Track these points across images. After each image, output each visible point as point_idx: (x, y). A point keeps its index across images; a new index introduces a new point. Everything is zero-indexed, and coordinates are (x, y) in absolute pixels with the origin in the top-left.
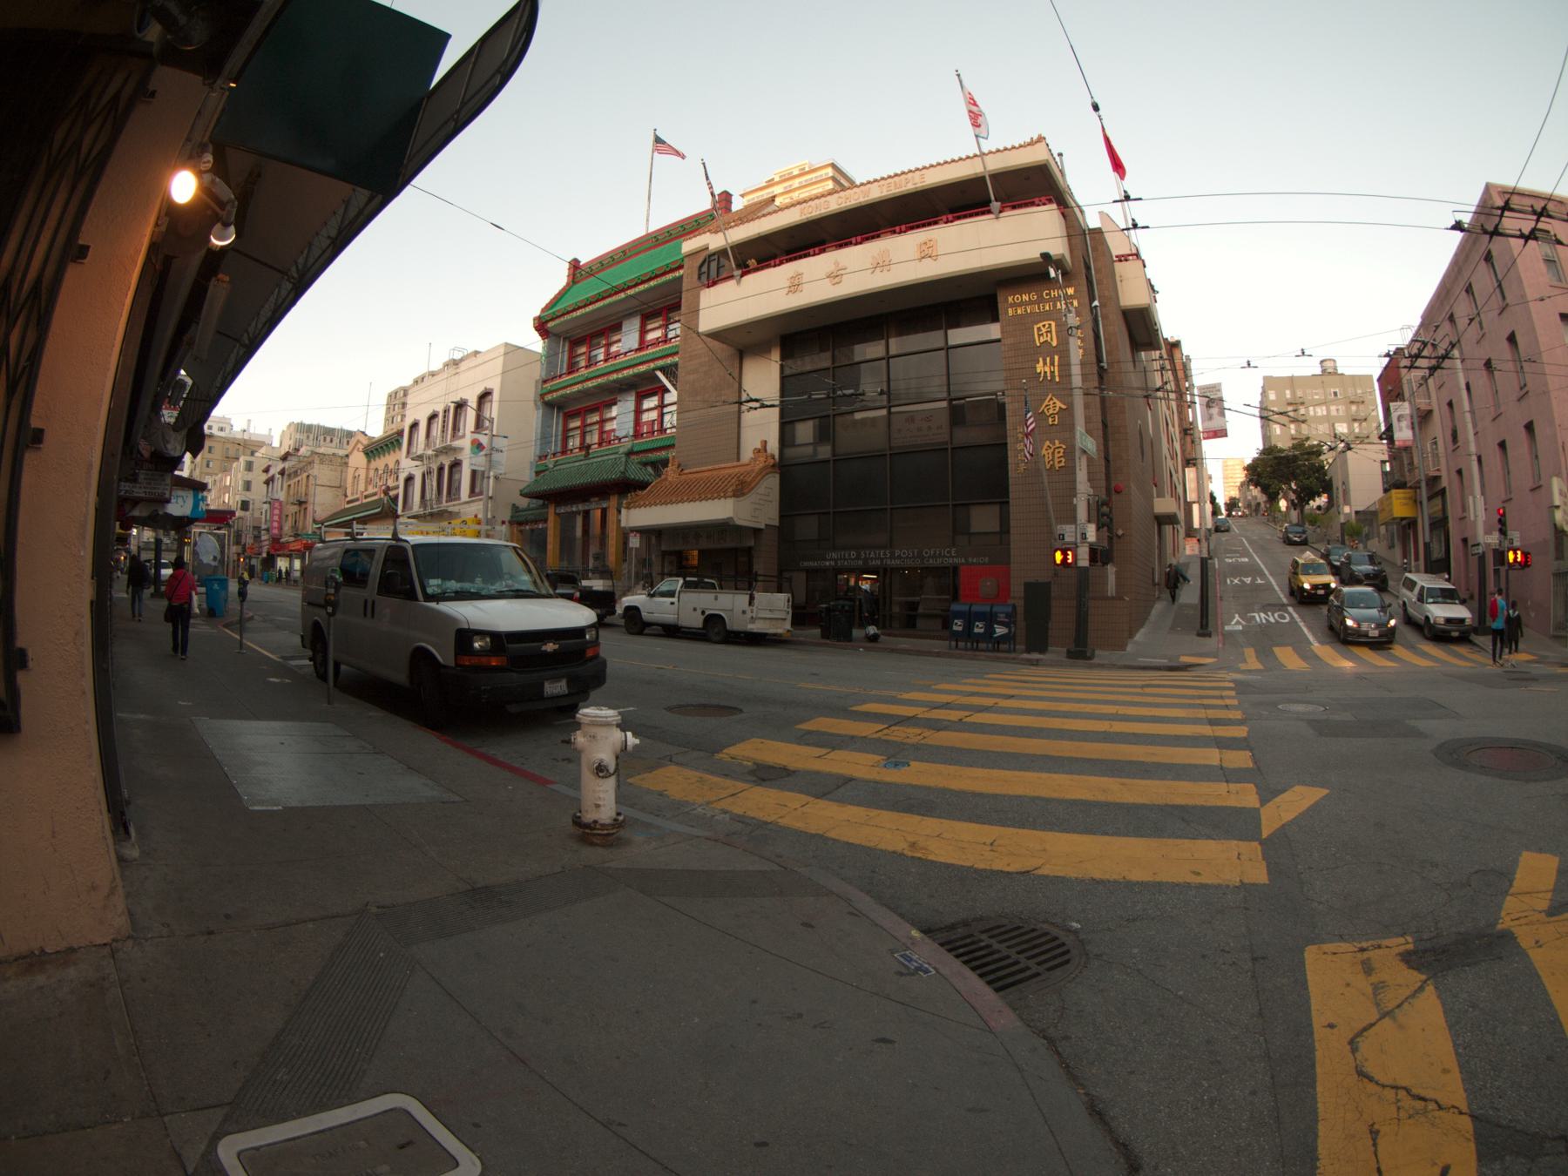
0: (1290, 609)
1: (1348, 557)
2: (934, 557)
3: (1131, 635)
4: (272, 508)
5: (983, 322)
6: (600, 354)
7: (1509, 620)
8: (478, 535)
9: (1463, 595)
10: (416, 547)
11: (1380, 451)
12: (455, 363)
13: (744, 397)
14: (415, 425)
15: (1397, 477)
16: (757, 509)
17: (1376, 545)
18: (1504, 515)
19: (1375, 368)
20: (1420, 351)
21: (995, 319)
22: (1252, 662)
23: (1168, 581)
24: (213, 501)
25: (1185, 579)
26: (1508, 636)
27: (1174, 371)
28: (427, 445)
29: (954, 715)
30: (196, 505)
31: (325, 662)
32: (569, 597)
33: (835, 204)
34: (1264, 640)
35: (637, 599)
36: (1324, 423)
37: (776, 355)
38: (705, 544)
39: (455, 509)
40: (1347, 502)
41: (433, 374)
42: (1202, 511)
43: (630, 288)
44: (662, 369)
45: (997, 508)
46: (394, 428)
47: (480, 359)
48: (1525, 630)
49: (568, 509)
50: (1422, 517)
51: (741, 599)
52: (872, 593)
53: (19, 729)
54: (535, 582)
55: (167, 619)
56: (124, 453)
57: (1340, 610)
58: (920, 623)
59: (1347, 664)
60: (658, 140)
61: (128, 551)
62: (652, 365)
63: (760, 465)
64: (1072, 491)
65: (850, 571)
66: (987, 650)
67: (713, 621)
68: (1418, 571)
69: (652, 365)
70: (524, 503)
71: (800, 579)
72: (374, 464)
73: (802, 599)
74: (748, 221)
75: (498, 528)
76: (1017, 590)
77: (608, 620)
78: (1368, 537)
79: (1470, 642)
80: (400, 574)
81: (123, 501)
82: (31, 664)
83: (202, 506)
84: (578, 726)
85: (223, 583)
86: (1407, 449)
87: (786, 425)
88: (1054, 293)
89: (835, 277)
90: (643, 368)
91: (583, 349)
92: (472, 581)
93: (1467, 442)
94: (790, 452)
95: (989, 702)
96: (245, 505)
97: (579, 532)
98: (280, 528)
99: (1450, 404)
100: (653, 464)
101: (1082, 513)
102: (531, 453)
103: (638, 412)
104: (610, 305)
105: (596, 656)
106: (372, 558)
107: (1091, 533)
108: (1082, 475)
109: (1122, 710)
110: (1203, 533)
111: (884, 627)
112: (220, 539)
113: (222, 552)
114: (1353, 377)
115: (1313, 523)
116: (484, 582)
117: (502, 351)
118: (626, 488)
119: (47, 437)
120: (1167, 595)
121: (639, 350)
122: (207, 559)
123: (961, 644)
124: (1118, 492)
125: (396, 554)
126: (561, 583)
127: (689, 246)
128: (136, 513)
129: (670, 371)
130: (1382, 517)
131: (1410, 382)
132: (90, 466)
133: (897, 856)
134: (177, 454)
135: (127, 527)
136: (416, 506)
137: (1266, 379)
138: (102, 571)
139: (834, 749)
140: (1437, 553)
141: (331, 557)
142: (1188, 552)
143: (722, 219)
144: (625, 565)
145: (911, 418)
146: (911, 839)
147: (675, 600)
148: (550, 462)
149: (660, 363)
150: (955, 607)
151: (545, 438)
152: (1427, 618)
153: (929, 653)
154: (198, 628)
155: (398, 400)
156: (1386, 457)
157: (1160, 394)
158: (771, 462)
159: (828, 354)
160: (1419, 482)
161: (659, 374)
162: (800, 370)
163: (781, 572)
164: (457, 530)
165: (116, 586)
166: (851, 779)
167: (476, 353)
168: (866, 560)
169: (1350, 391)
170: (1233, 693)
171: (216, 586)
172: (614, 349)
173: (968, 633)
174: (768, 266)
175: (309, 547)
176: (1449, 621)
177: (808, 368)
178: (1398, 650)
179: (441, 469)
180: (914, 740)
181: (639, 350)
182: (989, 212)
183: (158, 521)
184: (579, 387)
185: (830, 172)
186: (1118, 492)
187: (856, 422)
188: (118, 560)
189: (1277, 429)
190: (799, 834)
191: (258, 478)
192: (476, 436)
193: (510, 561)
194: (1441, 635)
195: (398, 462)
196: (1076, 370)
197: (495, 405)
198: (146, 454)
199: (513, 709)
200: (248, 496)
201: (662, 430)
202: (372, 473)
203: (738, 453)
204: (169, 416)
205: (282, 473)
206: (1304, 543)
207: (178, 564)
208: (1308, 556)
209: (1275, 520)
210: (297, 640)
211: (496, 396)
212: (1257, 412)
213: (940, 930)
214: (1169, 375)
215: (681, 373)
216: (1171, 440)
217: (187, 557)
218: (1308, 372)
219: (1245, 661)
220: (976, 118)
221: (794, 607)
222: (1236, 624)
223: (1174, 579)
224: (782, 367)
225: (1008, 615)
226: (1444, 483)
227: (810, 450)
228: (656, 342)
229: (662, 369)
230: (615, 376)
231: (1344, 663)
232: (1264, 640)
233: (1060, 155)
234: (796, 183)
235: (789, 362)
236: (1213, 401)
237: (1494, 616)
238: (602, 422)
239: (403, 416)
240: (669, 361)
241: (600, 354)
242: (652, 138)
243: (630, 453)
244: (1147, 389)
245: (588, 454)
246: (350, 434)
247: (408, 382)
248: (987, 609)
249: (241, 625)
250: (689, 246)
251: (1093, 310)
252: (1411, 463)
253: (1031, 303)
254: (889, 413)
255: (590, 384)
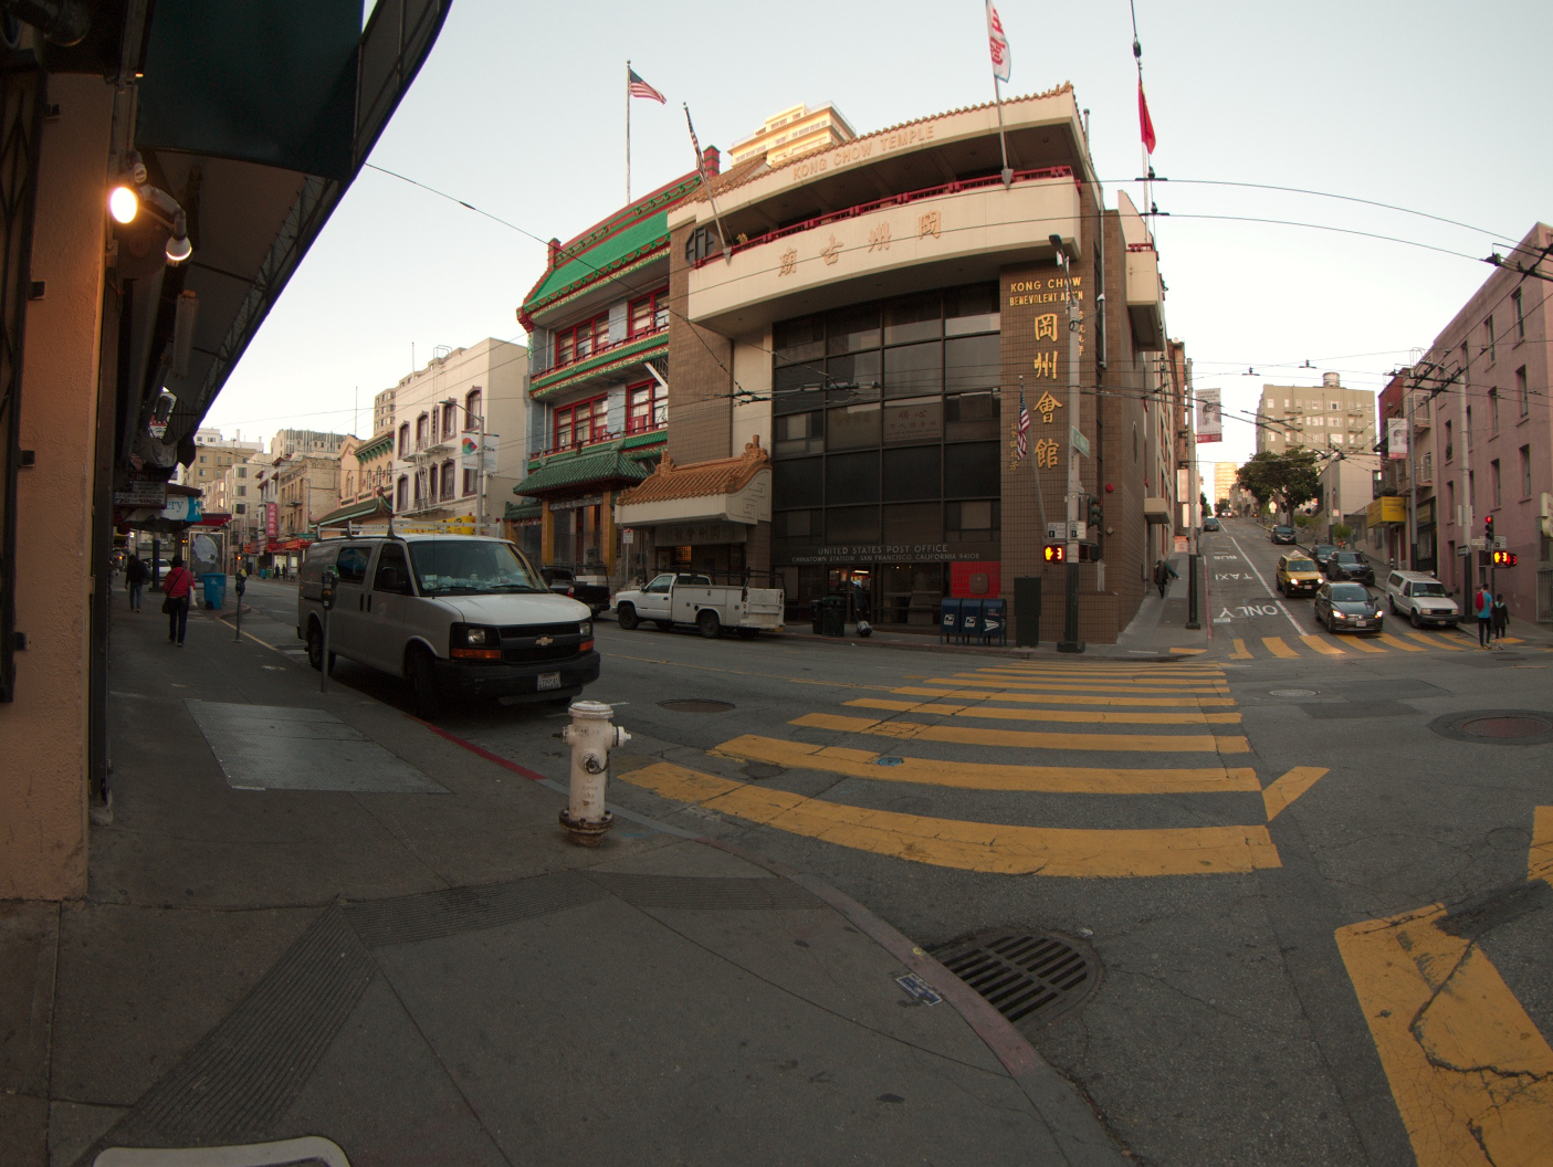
0: (1278, 603)
1: (1336, 556)
2: (926, 553)
3: (1121, 629)
4: (268, 511)
5: (983, 312)
6: (588, 346)
7: (1494, 610)
8: (473, 532)
9: (1448, 591)
10: (411, 545)
11: (1375, 461)
12: (440, 362)
13: (736, 391)
14: (405, 427)
15: (1387, 486)
16: (750, 505)
17: (1363, 546)
18: (1492, 522)
19: (1378, 384)
20: (1426, 373)
21: (996, 309)
22: (1241, 651)
23: (1157, 577)
24: (208, 505)
25: (1174, 575)
26: (1496, 623)
27: (1174, 373)
28: (419, 446)
29: (947, 710)
30: (192, 510)
31: (320, 653)
32: (564, 592)
33: (832, 164)
34: (1253, 631)
35: (630, 594)
36: (1319, 433)
37: (768, 344)
38: (697, 540)
39: (450, 508)
40: (1336, 506)
41: (419, 375)
42: (1192, 511)
43: (614, 271)
44: (652, 361)
45: (987, 506)
46: (385, 430)
47: (465, 357)
48: (1511, 618)
49: (562, 506)
50: (1411, 519)
51: (734, 595)
52: (864, 588)
53: (11, 700)
54: (530, 578)
55: (165, 611)
56: (116, 466)
57: (1327, 603)
58: (912, 618)
59: (1336, 652)
60: (633, 78)
61: (127, 552)
62: (642, 357)
63: (752, 460)
64: (1064, 490)
65: (841, 566)
66: (978, 644)
67: (706, 616)
68: (1404, 569)
69: (642, 357)
70: (517, 500)
71: (792, 575)
72: (367, 467)
73: (794, 595)
74: (738, 186)
75: (492, 525)
76: (1007, 585)
77: (602, 614)
78: (1356, 538)
79: (1458, 629)
80: (396, 570)
81: (118, 509)
82: (28, 646)
83: (198, 511)
84: (570, 720)
85: (221, 579)
86: (1400, 461)
87: (779, 419)
88: (1059, 283)
89: (830, 255)
90: (632, 361)
91: (570, 342)
92: (468, 577)
93: (1461, 458)
94: (783, 447)
95: (981, 695)
96: (240, 509)
97: (573, 529)
98: (277, 529)
99: (1448, 424)
100: (646, 460)
101: (1072, 512)
102: (523, 451)
103: (630, 407)
104: (595, 291)
105: (590, 650)
106: (368, 555)
107: (1082, 531)
108: (1074, 475)
109: (1115, 701)
110: (1192, 532)
111: (876, 622)
112: (218, 540)
113: (220, 551)
114: (1354, 391)
115: (1302, 524)
116: (479, 577)
117: (487, 347)
118: (619, 484)
119: (38, 457)
120: (1155, 590)
121: (628, 340)
122: (205, 558)
123: (952, 639)
124: (1109, 491)
125: (392, 551)
126: (556, 578)
127: (675, 218)
128: (133, 518)
129: (660, 363)
130: (1370, 521)
131: (1411, 400)
132: (84, 480)
133: (894, 860)
134: (170, 465)
135: (125, 529)
136: (411, 506)
137: (1266, 387)
138: (101, 568)
139: (827, 745)
140: (1424, 553)
141: (328, 555)
142: (1177, 550)
143: (709, 183)
144: (619, 561)
145: (904, 413)
146: (907, 841)
147: (668, 595)
148: (542, 460)
149: (650, 354)
150: (946, 602)
151: (536, 436)
152: (1414, 609)
153: (921, 648)
154: (195, 619)
155: (386, 403)
156: (1378, 468)
157: (1157, 396)
158: (763, 457)
159: (821, 344)
160: (1409, 491)
161: (649, 366)
162: (793, 361)
163: (773, 567)
164: (452, 528)
165: (114, 582)
166: (842, 778)
167: (461, 350)
168: (857, 556)
169: (1350, 405)
170: (1224, 682)
171: (214, 582)
172: (602, 340)
173: (959, 627)
174: (760, 242)
175: (306, 546)
176: (1435, 612)
177: (802, 358)
178: (1386, 638)
179: (434, 469)
180: (907, 735)
181: (628, 340)
182: (1000, 181)
183: (155, 524)
184: (568, 382)
185: (827, 119)
186: (1109, 491)
187: (849, 417)
188: (117, 560)
189: (1272, 436)
190: (792, 836)
191: (252, 483)
192: (467, 436)
193: (505, 557)
194: (1427, 624)
195: (390, 464)
196: (1074, 367)
197: (485, 404)
198: (139, 467)
199: (505, 701)
200: (243, 500)
201: (654, 426)
202: (365, 475)
203: (731, 449)
204: (157, 431)
205: (276, 477)
206: (1292, 543)
207: (176, 562)
208: (1296, 554)
209: (1264, 521)
210: (293, 631)
211: (484, 394)
212: (1253, 419)
213: (943, 945)
214: (1169, 378)
215: (671, 364)
216: (1165, 442)
217: (185, 556)
218: (1310, 384)
219: (1234, 651)
220: (998, 49)
221: (787, 603)
222: (1224, 617)
223: (1163, 575)
224: (774, 357)
225: (998, 610)
226: (1434, 493)
227: (802, 445)
228: (645, 332)
229: (652, 361)
230: (604, 370)
231: (1334, 651)
232: (1253, 631)
233: (1087, 112)
234: (789, 135)
235: (782, 352)
236: (1211, 405)
237: (1480, 606)
238: (593, 418)
239: (393, 419)
240: (659, 352)
241: (588, 346)
242: (626, 76)
243: (622, 450)
244: (1145, 390)
245: (580, 451)
246: (340, 439)
247: (394, 384)
248: (977, 603)
249: (239, 616)
250: (675, 218)
251: (1098, 303)
252: (1403, 474)
253: (1034, 292)
254: (883, 407)
255: (579, 379)
